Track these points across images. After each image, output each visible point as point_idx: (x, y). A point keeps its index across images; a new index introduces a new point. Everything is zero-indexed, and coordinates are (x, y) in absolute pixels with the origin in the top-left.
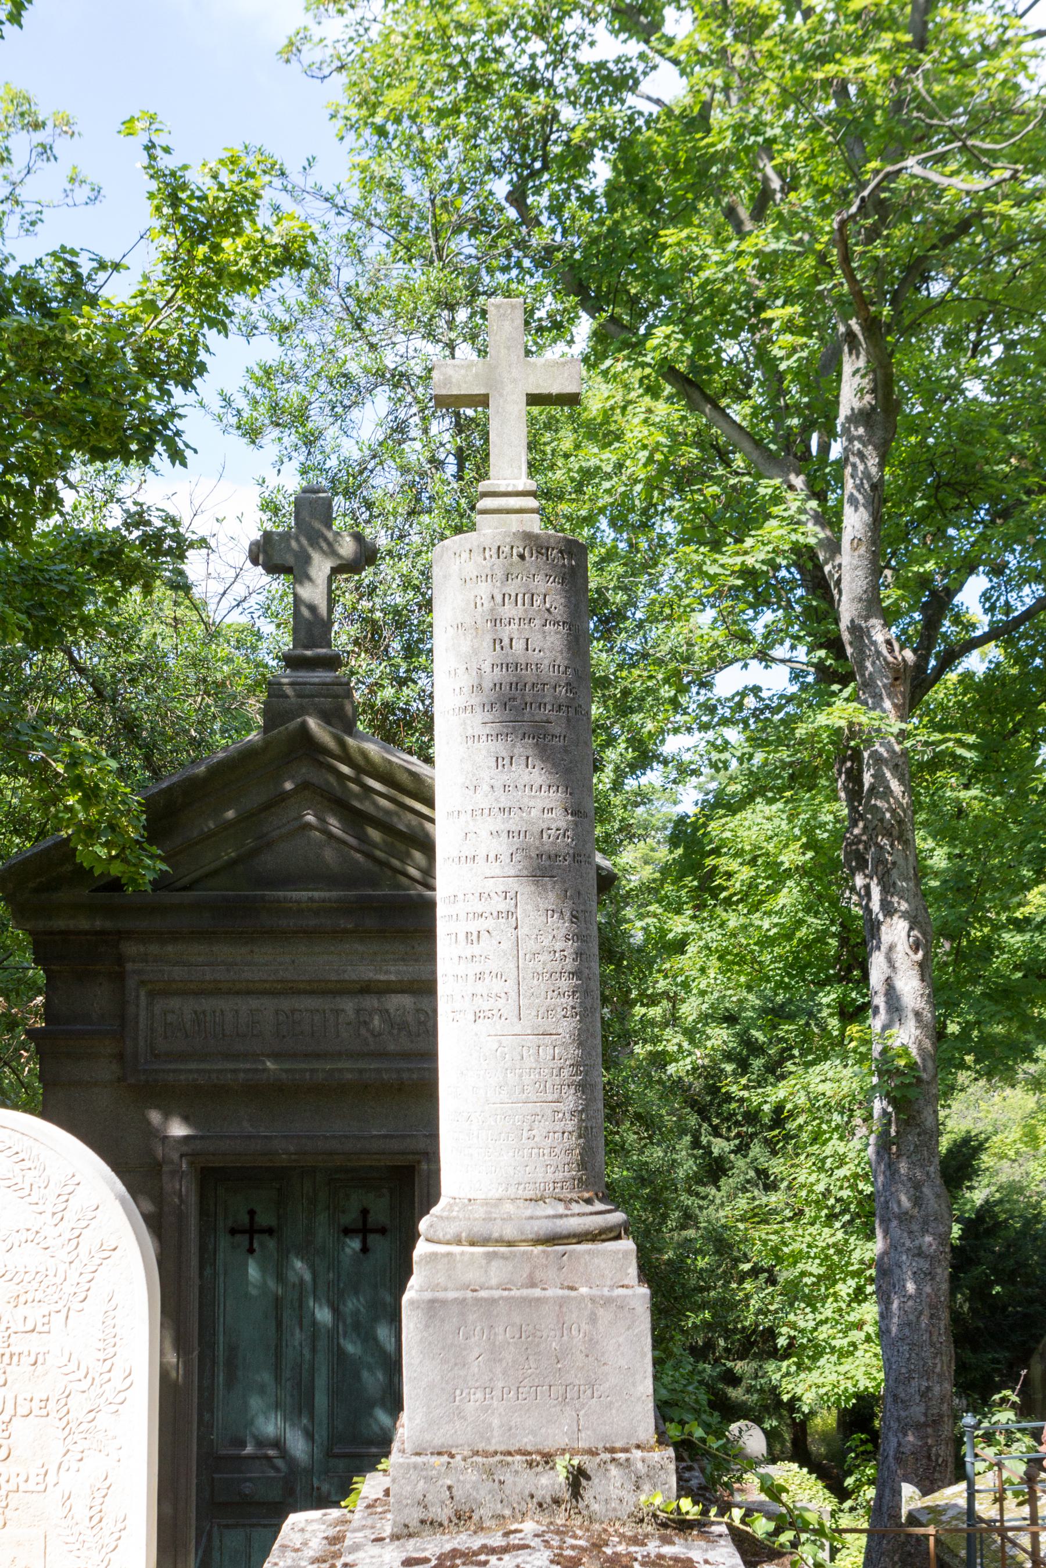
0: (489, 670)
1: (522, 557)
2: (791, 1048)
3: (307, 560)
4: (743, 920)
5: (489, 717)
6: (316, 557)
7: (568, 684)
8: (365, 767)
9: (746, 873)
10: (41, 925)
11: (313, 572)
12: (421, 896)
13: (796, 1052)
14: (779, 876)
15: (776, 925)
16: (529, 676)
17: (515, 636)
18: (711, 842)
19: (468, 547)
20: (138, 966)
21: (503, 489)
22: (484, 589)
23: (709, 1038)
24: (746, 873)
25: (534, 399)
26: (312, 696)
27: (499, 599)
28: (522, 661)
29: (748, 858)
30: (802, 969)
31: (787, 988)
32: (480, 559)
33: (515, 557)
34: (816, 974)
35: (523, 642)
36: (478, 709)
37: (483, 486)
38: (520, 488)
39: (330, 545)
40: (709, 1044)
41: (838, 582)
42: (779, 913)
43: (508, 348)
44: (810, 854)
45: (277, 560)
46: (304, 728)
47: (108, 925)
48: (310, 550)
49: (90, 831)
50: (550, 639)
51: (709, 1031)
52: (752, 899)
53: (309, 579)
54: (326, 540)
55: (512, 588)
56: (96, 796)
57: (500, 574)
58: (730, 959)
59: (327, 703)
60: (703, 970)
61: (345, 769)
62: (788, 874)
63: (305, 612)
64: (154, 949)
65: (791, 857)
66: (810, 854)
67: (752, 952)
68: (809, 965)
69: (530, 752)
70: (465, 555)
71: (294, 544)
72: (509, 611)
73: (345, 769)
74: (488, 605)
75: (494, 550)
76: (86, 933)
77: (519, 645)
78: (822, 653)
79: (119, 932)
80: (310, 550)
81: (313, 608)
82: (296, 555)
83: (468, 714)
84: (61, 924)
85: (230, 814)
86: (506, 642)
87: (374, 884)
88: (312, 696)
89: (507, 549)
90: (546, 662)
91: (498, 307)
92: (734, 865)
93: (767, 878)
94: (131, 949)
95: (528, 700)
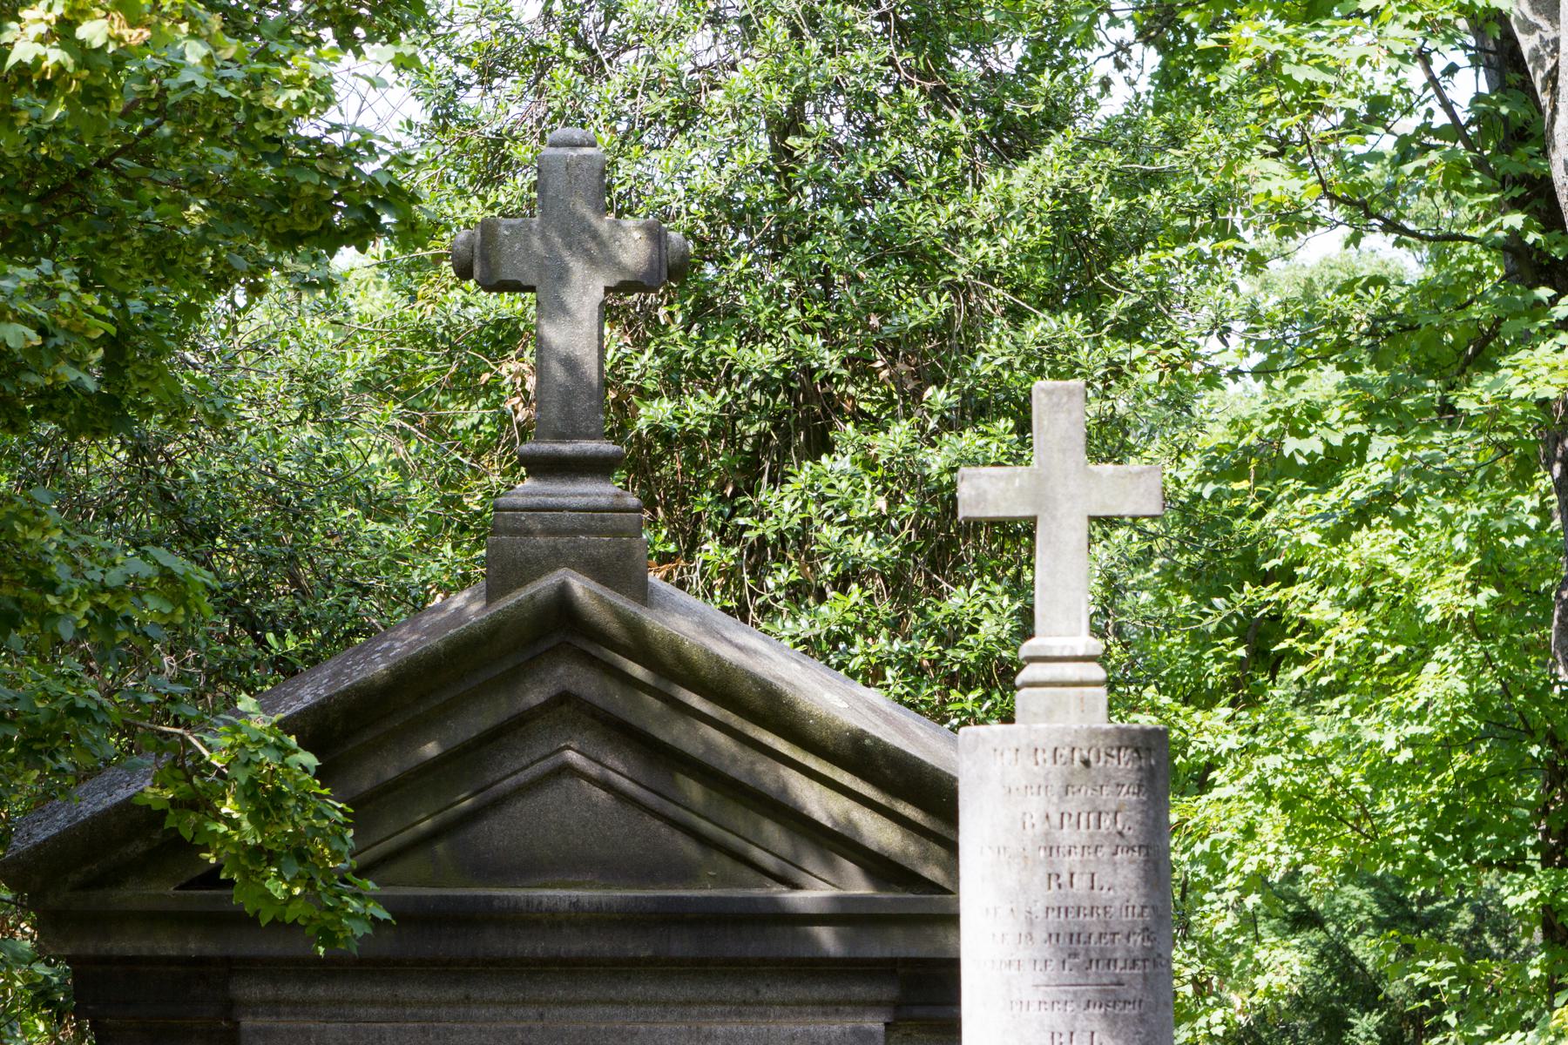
0: (1042, 914)
1: (1086, 763)
2: (1439, 1008)
3: (562, 276)
4: (1339, 731)
5: (1041, 978)
6: (577, 267)
7: (1146, 929)
8: (677, 668)
9: (1348, 629)
10: (90, 947)
11: (571, 299)
12: (773, 901)
13: (1450, 1018)
14: (1422, 643)
15: (1411, 742)
16: (1093, 924)
17: (1077, 870)
18: (1273, 553)
19: (1014, 744)
20: (263, 1022)
21: (1056, 653)
22: (1036, 806)
23: (1259, 969)
24: (1348, 629)
25: (1091, 518)
26: (573, 532)
27: (1055, 819)
28: (1087, 904)
29: (1355, 591)
30: (1467, 833)
31: (1431, 872)
32: (1030, 763)
33: (1077, 763)
34: (1498, 846)
35: (1087, 878)
36: (1028, 967)
37: (1027, 648)
38: (1080, 653)
39: (602, 244)
40: (1261, 982)
41: (1553, 77)
42: (1420, 715)
43: (1064, 451)
44: (1488, 592)
45: (507, 274)
46: (563, 591)
47: (211, 948)
48: (566, 255)
49: (261, 855)
50: (1122, 872)
51: (1260, 954)
52: (1364, 681)
53: (563, 309)
54: (595, 235)
55: (1073, 804)
56: (279, 808)
57: (1057, 785)
58: (1311, 812)
59: (602, 545)
60: (1249, 832)
61: (637, 670)
62: (1439, 633)
63: (558, 372)
64: (292, 991)
65: (1443, 597)
66: (1488, 592)
67: (1356, 796)
68: (1480, 824)
69: (1096, 1026)
70: (1009, 755)
71: (536, 243)
72: (1068, 836)
73: (637, 670)
74: (1041, 827)
75: (1049, 754)
76: (170, 961)
77: (1081, 883)
78: (1516, 220)
79: (228, 960)
80: (566, 255)
81: (571, 364)
82: (542, 267)
83: (1013, 971)
84: (125, 945)
85: (431, 749)
86: (1065, 878)
87: (686, 874)
88: (573, 532)
89: (1066, 752)
90: (1117, 904)
91: (1049, 393)
92: (1322, 612)
93: (1394, 640)
94: (248, 990)
95: (1094, 956)
